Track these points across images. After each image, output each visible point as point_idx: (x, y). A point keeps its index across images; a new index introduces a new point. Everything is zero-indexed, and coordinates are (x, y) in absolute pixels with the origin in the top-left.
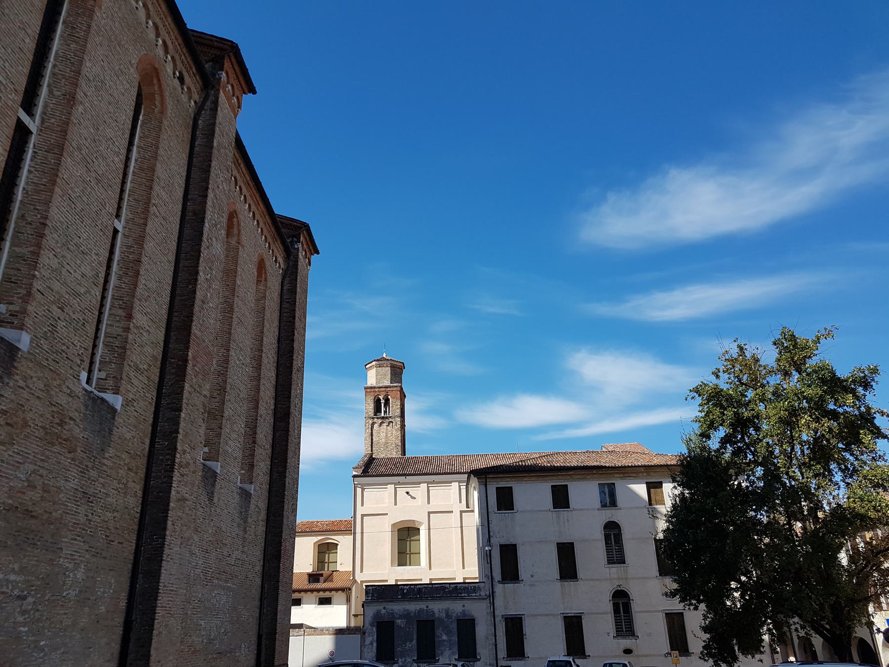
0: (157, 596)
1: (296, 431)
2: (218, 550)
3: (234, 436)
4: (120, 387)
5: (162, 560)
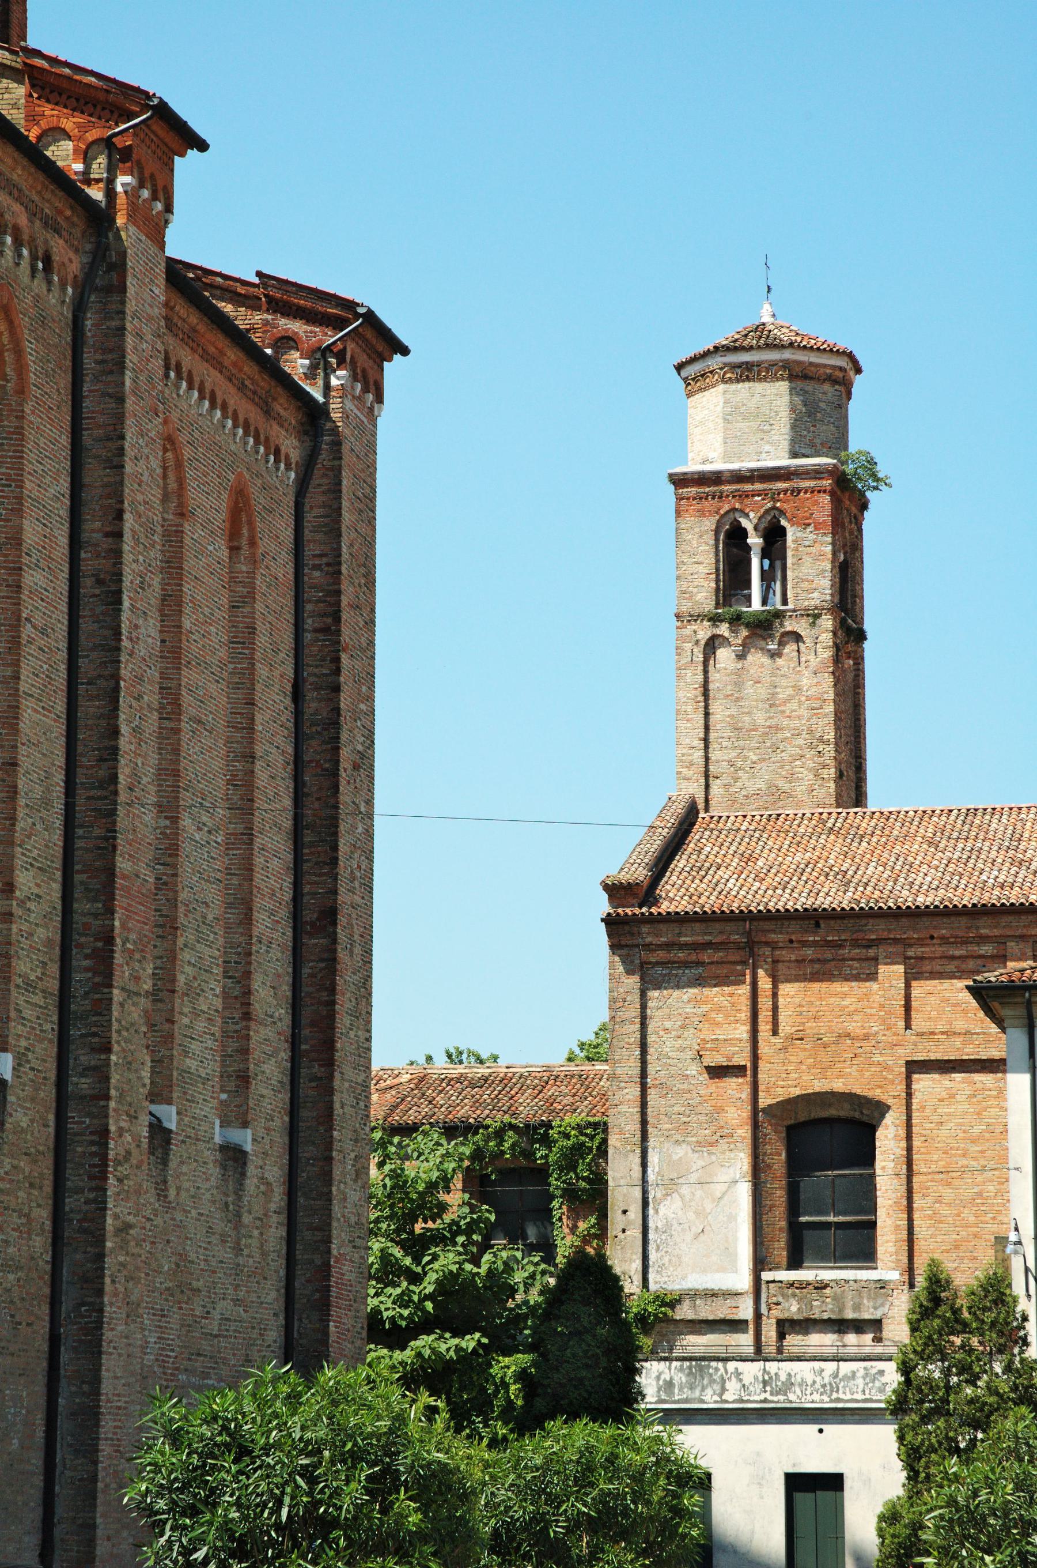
0: (98, 1420)
1: (357, 950)
2: (184, 1306)
3: (201, 1025)
4: (7, 1036)
5: (100, 1353)
